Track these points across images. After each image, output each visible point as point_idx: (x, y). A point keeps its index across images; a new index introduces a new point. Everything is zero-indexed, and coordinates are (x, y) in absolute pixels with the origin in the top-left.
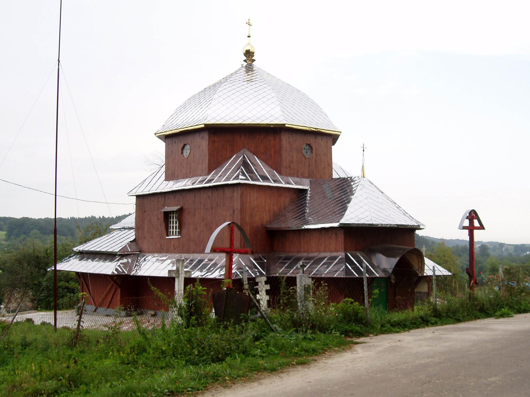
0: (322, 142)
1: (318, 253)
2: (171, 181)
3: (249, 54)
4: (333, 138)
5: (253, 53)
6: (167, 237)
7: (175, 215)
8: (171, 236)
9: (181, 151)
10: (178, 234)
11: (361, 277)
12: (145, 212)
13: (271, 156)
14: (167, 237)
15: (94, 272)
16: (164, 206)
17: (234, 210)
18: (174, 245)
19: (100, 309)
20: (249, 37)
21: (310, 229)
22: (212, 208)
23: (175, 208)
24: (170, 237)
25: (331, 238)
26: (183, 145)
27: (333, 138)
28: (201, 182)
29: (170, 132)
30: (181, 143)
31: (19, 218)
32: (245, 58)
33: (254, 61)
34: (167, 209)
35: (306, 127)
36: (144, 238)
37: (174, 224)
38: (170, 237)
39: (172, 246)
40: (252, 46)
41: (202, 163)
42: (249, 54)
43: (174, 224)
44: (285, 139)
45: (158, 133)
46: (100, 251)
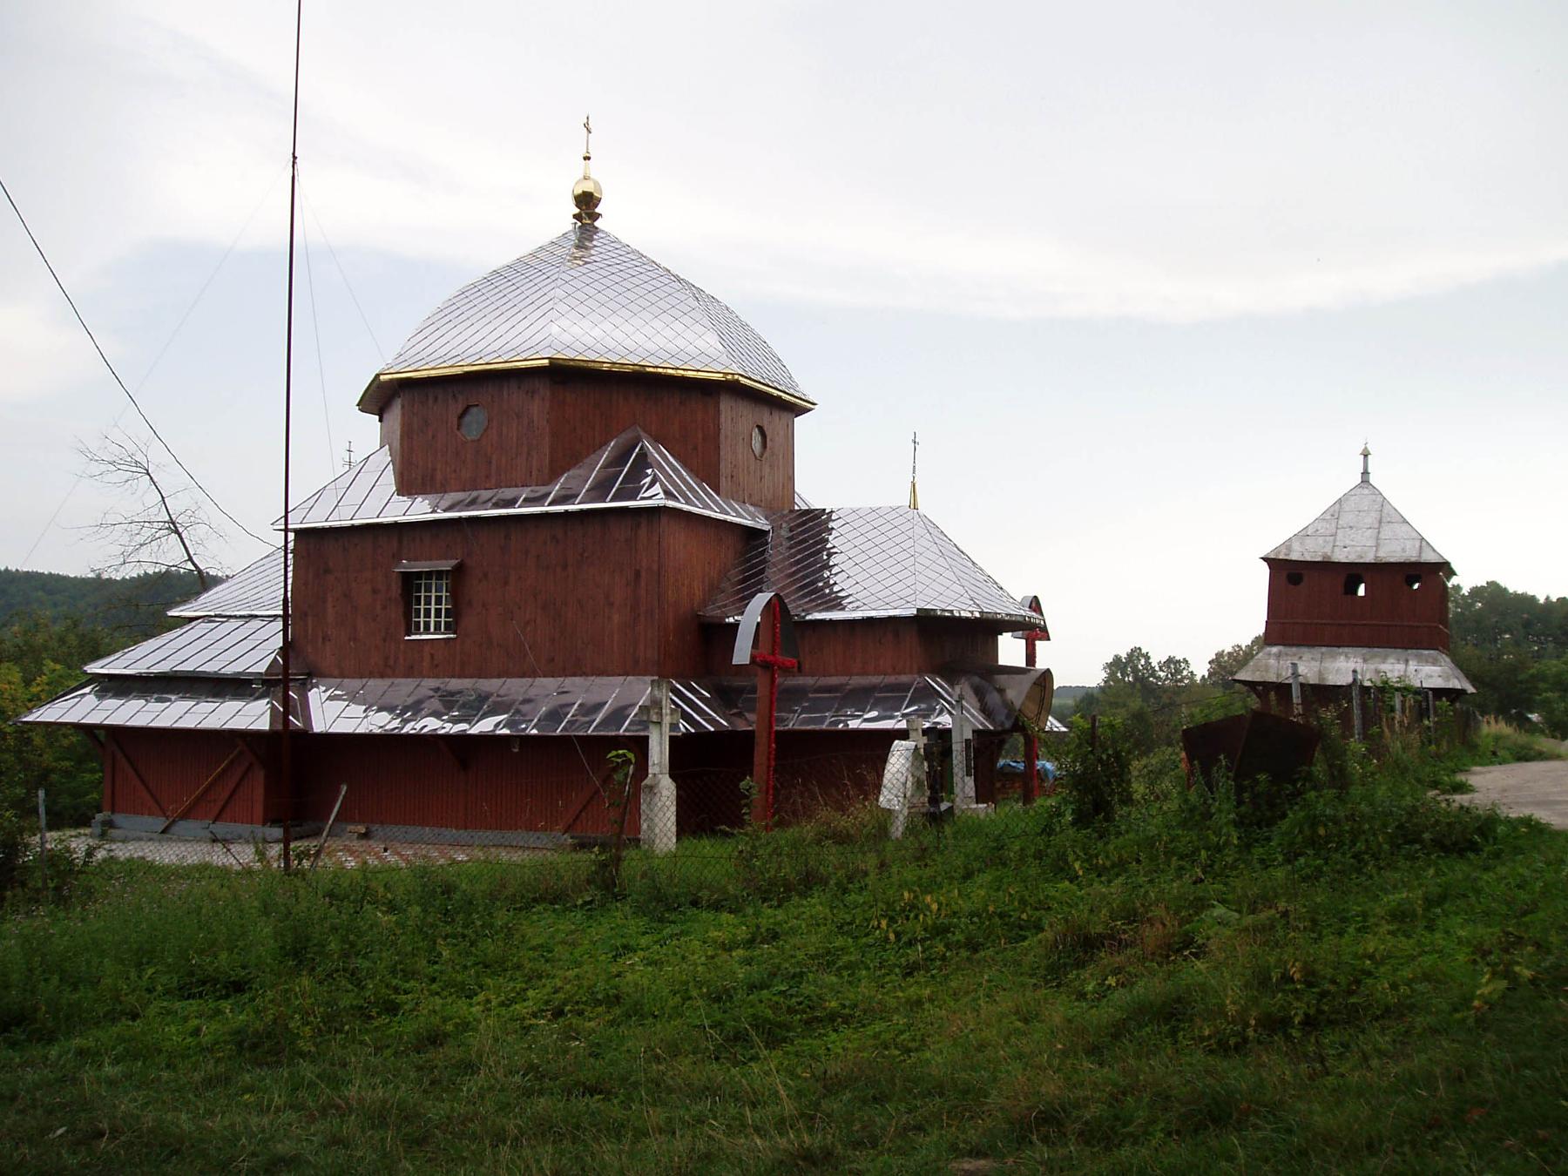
0: (734, 419)
1: (847, 678)
2: (420, 499)
3: (587, 203)
4: (794, 408)
5: (599, 200)
6: (407, 638)
7: (444, 582)
8: (421, 634)
9: (455, 421)
10: (446, 629)
11: (642, 734)
12: (327, 571)
13: (695, 448)
14: (407, 638)
15: (152, 725)
16: (397, 558)
17: (637, 574)
18: (432, 655)
19: (182, 826)
20: (587, 158)
21: (831, 620)
22: (565, 567)
23: (446, 565)
24: (413, 637)
25: (880, 643)
26: (465, 406)
27: (794, 408)
28: (538, 500)
29: (433, 373)
30: (457, 401)
31: (1268, 570)
32: (577, 211)
33: (597, 216)
34: (407, 566)
35: (750, 379)
36: (323, 639)
37: (433, 604)
38: (413, 637)
39: (427, 658)
40: (596, 184)
41: (529, 454)
42: (587, 203)
43: (433, 604)
44: (729, 410)
45: (392, 371)
46: (194, 671)
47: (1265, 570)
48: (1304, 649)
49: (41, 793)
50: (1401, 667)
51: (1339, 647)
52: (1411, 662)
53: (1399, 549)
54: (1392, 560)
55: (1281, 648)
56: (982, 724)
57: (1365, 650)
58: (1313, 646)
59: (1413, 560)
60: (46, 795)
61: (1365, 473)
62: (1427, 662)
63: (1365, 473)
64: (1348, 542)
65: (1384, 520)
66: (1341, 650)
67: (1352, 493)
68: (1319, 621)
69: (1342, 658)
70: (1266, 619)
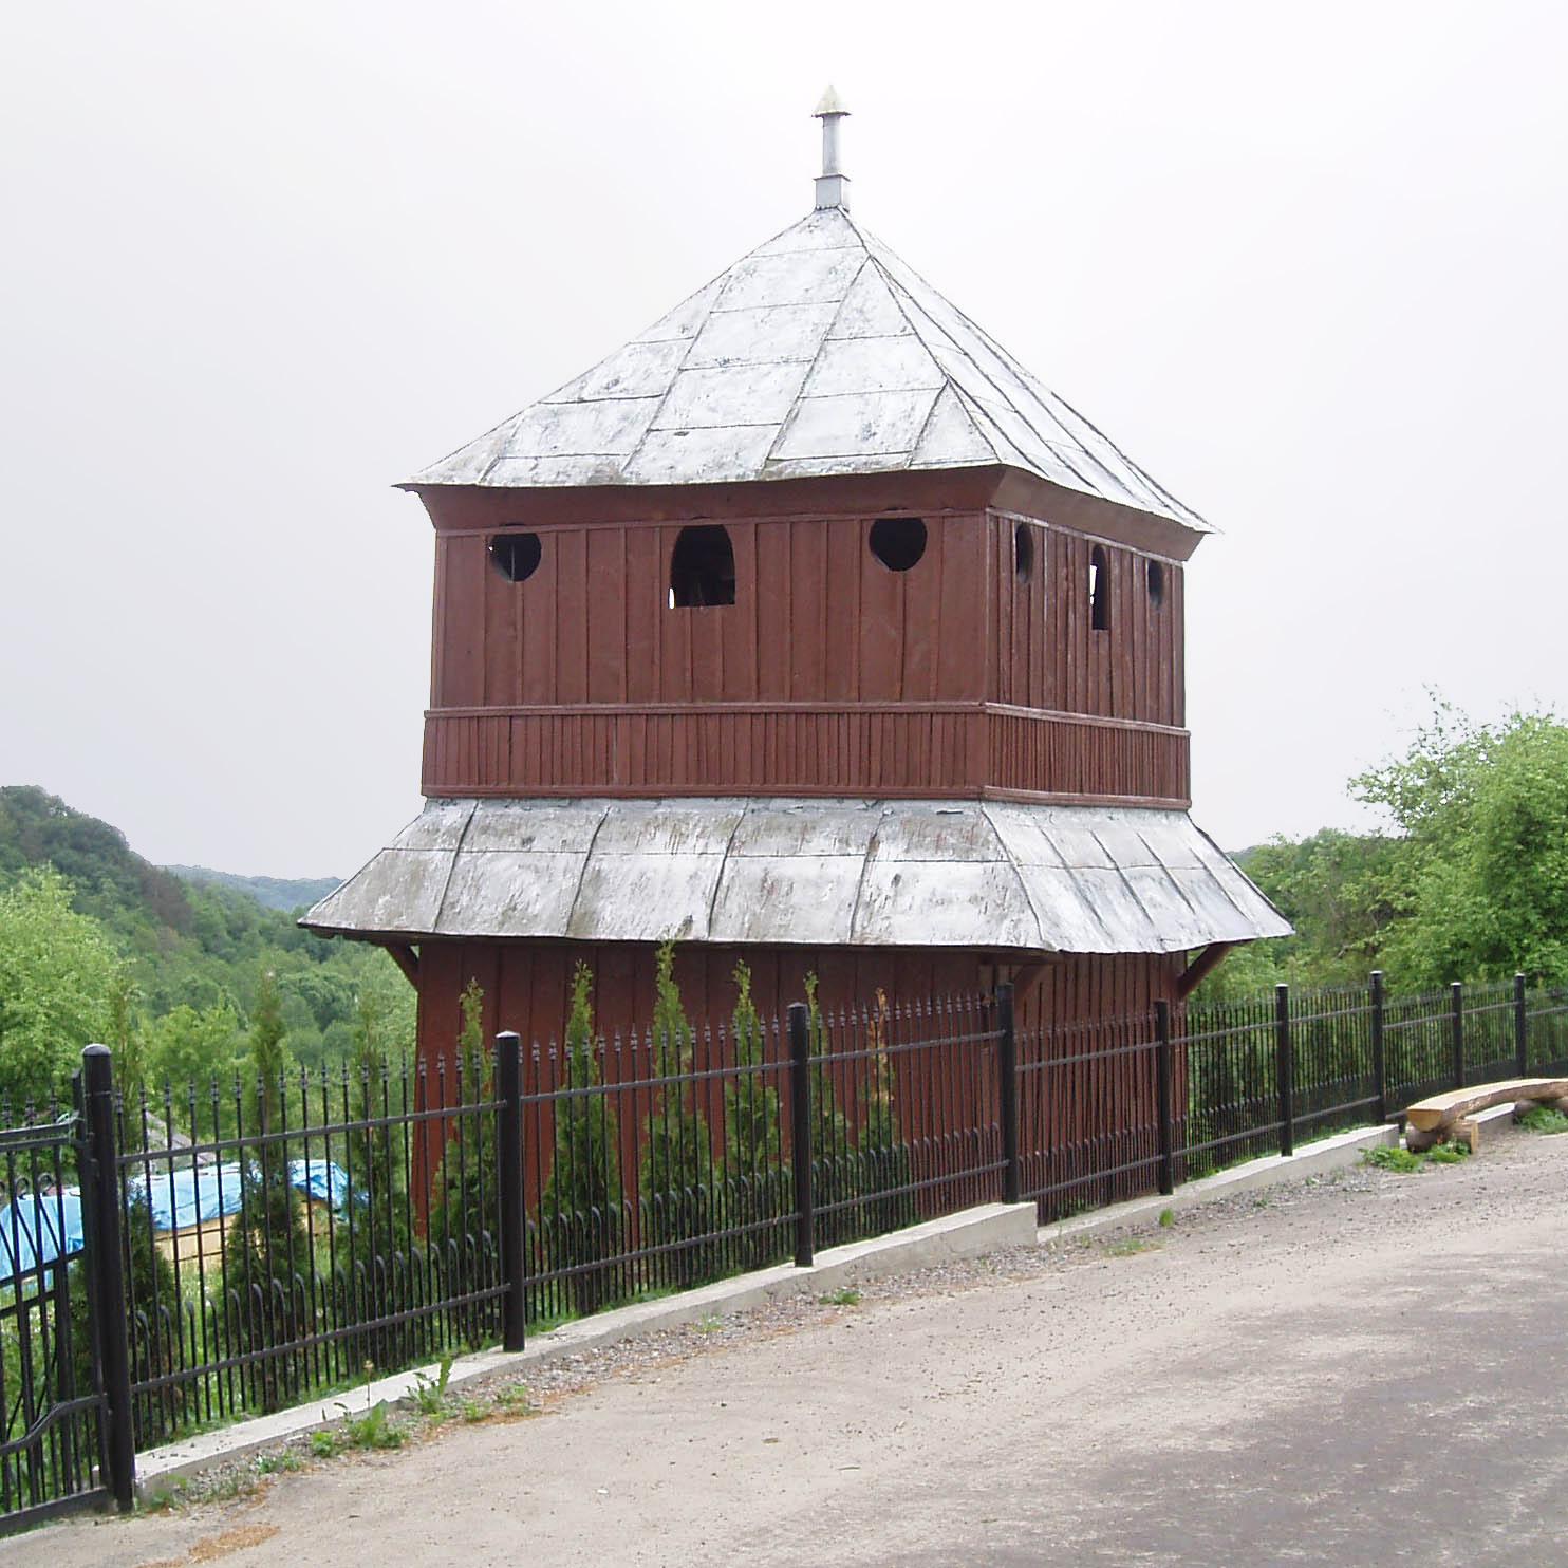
47: (419, 534)
48: (548, 811)
49: (276, 1281)
50: (849, 867)
51: (658, 797)
52: (883, 849)
53: (856, 427)
54: (817, 470)
55: (468, 806)
56: (1497, 1100)
57: (737, 808)
58: (576, 798)
59: (891, 463)
60: (280, 1279)
61: (831, 176)
62: (939, 844)
63: (831, 176)
64: (699, 415)
65: (841, 330)
66: (665, 809)
67: (767, 251)
68: (944, 704)
69: (662, 837)
70: (426, 704)
